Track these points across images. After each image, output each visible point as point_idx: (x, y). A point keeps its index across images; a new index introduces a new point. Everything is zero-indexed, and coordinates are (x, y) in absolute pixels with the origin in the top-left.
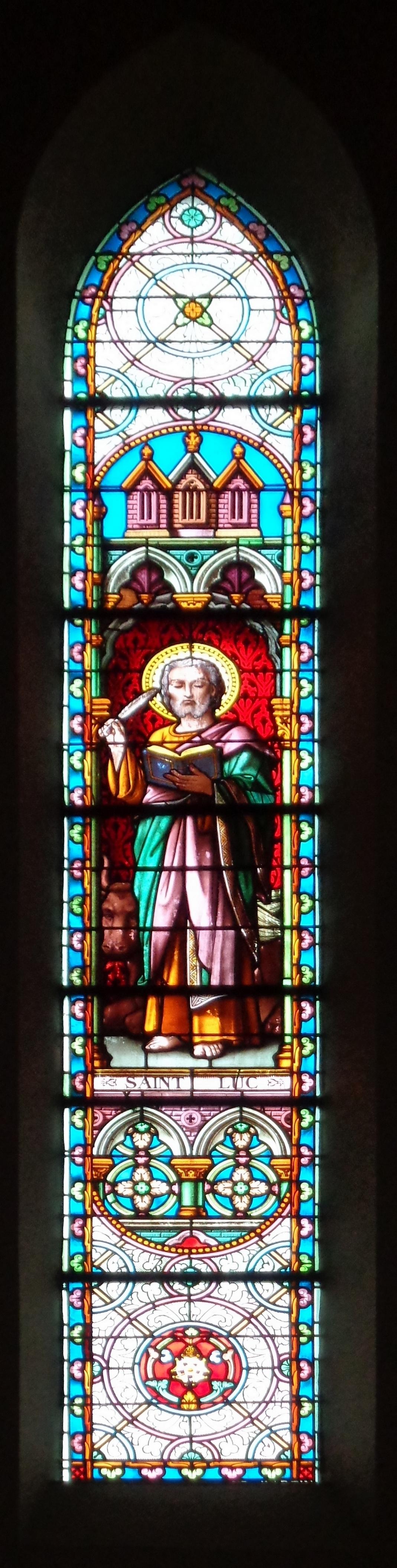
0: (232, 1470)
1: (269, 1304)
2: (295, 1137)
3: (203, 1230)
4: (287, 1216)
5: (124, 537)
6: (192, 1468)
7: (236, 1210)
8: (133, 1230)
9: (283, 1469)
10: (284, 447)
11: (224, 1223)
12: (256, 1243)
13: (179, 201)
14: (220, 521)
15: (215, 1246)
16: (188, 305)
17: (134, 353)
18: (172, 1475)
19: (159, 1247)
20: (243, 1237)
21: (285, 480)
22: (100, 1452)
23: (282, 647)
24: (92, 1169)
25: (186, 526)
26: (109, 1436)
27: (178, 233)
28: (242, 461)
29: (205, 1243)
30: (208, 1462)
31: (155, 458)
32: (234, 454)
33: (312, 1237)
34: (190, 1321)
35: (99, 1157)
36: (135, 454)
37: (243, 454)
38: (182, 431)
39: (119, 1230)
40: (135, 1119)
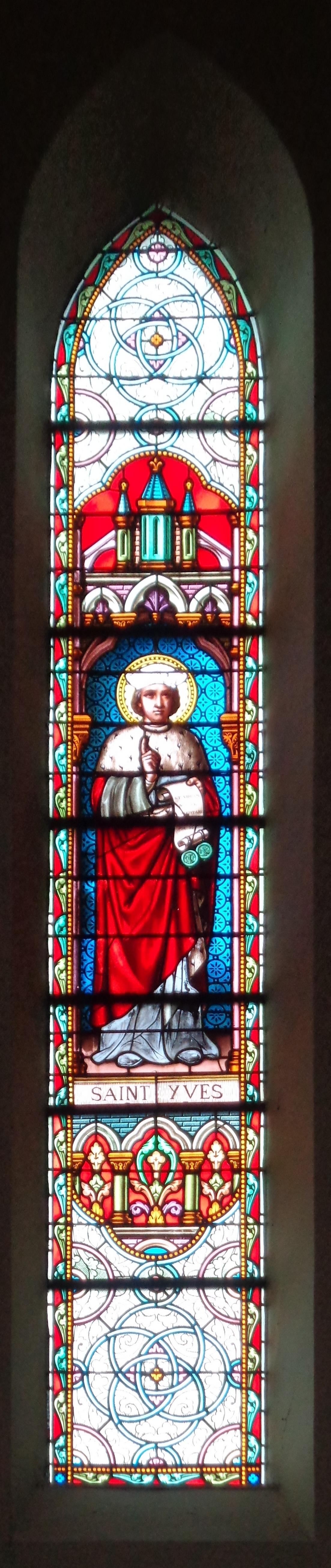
35: (78, 1152)
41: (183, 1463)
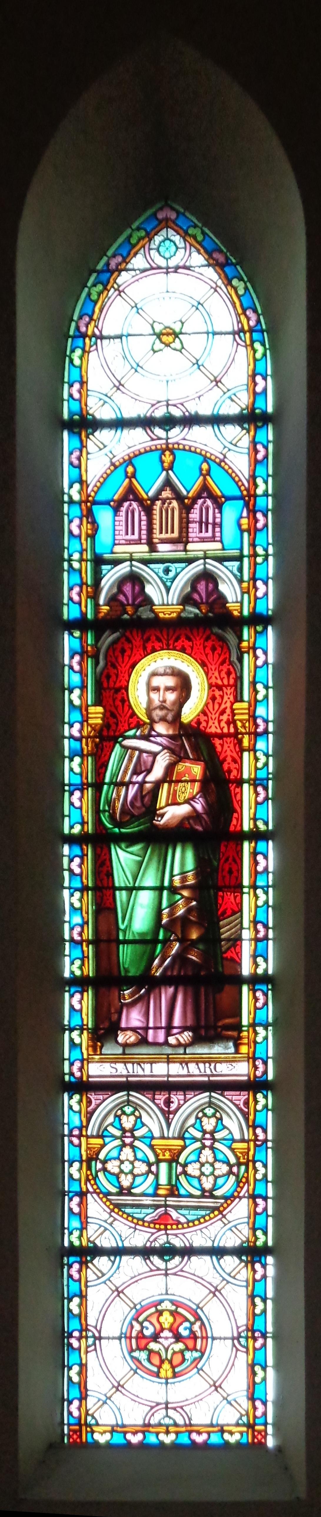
0: (199, 1435)
2: (251, 1117)
3: (176, 1208)
4: (244, 1197)
5: (112, 553)
6: (167, 1432)
7: (121, 1188)
8: (119, 1206)
9: (241, 1433)
10: (241, 463)
11: (192, 1202)
12: (221, 1219)
13: (156, 234)
14: (190, 535)
15: (185, 1223)
20: (209, 1215)
22: (93, 1417)
24: (88, 1148)
25: (163, 541)
26: (101, 1402)
27: (155, 264)
31: (138, 475)
32: (201, 470)
33: (265, 1213)
34: (167, 1294)
39: (108, 1207)
40: (123, 1102)
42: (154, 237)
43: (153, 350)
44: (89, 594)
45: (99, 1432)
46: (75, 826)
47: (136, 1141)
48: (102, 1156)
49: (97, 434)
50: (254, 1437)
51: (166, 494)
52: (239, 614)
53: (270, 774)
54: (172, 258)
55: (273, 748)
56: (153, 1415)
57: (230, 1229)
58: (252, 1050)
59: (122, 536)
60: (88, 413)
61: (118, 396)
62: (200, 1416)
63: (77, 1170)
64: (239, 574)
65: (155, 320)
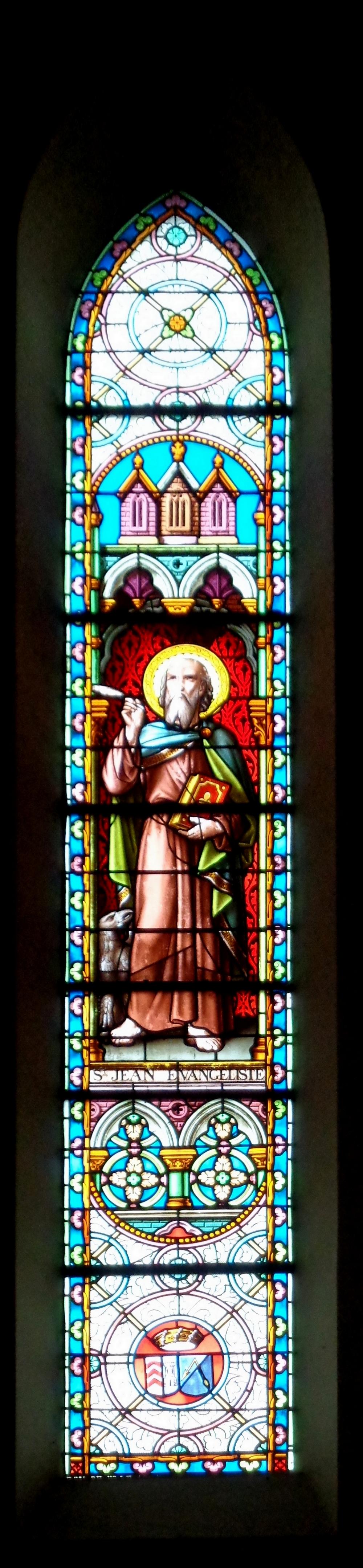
1: (248, 1298)
2: (270, 1127)
5: (118, 544)
6: (179, 1462)
9: (260, 1461)
10: (256, 457)
12: (236, 1232)
13: (164, 222)
15: (200, 1236)
16: (172, 319)
17: (125, 364)
18: (160, 1468)
19: (149, 1237)
20: (225, 1227)
21: (257, 486)
22: (98, 1448)
23: (258, 649)
24: (90, 1161)
25: (172, 534)
28: (221, 470)
29: (191, 1234)
30: (193, 1455)
31: (145, 467)
32: (214, 463)
36: (127, 463)
37: (222, 466)
38: (166, 441)
39: (113, 1220)
41: (206, 1450)
42: (161, 224)
43: (162, 336)
44: (93, 586)
45: (103, 1463)
46: (75, 1176)
47: (144, 1152)
48: (106, 1169)
49: (102, 421)
50: (274, 1465)
51: (176, 486)
52: (255, 611)
53: (291, 1446)
54: (181, 246)
55: (291, 917)
56: (163, 1443)
57: (248, 1429)
58: (269, 1057)
59: (128, 527)
60: (92, 399)
61: (125, 383)
62: (216, 1444)
63: (79, 1111)
64: (255, 570)
65: (165, 306)
